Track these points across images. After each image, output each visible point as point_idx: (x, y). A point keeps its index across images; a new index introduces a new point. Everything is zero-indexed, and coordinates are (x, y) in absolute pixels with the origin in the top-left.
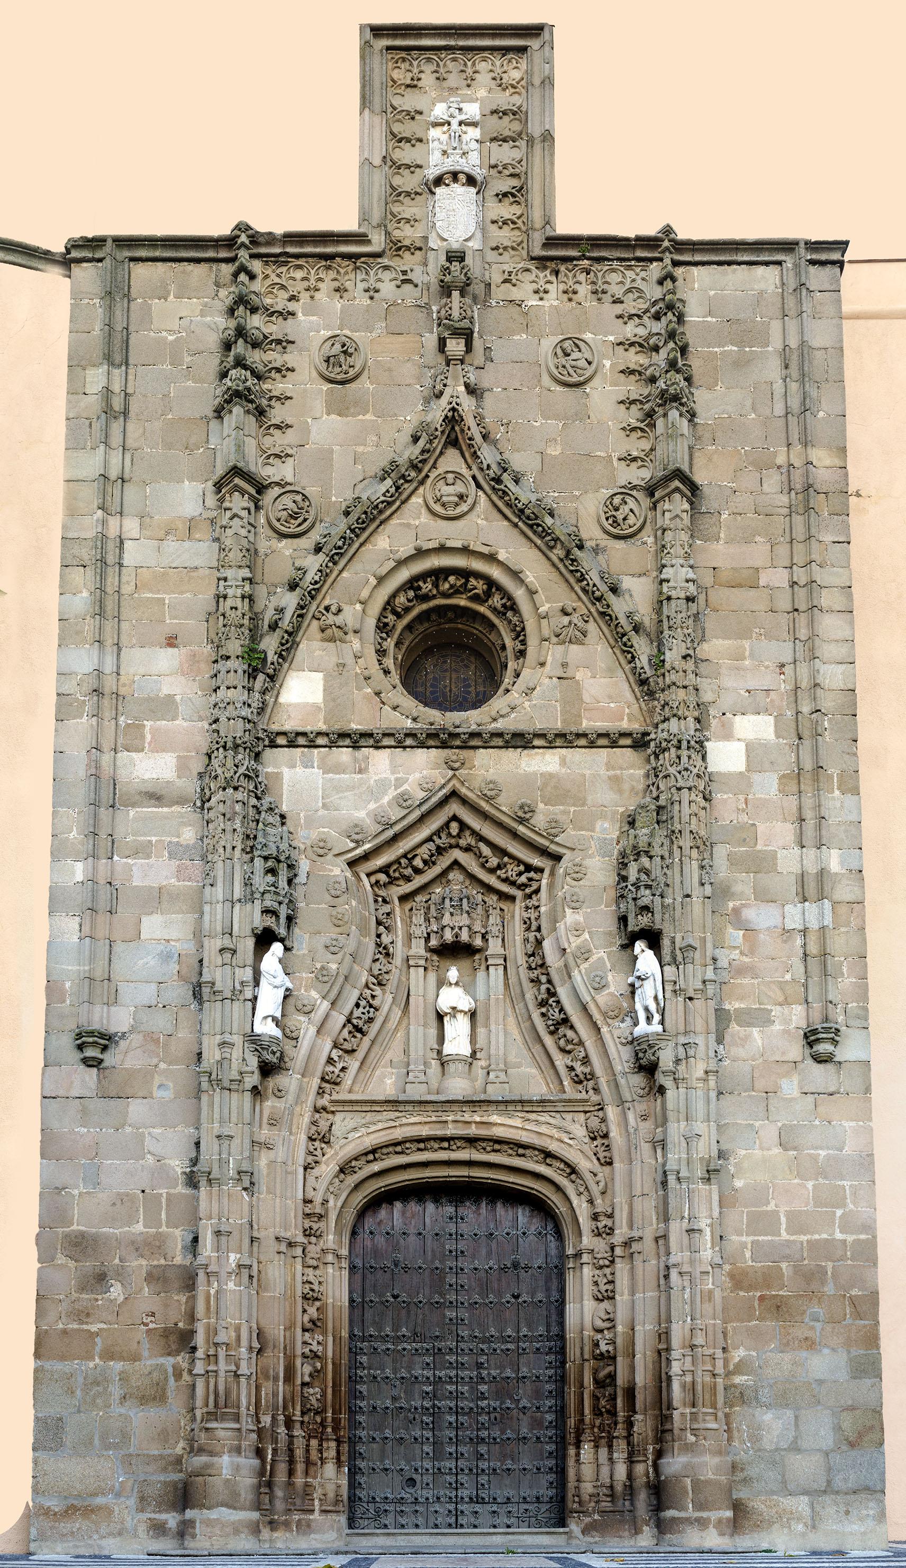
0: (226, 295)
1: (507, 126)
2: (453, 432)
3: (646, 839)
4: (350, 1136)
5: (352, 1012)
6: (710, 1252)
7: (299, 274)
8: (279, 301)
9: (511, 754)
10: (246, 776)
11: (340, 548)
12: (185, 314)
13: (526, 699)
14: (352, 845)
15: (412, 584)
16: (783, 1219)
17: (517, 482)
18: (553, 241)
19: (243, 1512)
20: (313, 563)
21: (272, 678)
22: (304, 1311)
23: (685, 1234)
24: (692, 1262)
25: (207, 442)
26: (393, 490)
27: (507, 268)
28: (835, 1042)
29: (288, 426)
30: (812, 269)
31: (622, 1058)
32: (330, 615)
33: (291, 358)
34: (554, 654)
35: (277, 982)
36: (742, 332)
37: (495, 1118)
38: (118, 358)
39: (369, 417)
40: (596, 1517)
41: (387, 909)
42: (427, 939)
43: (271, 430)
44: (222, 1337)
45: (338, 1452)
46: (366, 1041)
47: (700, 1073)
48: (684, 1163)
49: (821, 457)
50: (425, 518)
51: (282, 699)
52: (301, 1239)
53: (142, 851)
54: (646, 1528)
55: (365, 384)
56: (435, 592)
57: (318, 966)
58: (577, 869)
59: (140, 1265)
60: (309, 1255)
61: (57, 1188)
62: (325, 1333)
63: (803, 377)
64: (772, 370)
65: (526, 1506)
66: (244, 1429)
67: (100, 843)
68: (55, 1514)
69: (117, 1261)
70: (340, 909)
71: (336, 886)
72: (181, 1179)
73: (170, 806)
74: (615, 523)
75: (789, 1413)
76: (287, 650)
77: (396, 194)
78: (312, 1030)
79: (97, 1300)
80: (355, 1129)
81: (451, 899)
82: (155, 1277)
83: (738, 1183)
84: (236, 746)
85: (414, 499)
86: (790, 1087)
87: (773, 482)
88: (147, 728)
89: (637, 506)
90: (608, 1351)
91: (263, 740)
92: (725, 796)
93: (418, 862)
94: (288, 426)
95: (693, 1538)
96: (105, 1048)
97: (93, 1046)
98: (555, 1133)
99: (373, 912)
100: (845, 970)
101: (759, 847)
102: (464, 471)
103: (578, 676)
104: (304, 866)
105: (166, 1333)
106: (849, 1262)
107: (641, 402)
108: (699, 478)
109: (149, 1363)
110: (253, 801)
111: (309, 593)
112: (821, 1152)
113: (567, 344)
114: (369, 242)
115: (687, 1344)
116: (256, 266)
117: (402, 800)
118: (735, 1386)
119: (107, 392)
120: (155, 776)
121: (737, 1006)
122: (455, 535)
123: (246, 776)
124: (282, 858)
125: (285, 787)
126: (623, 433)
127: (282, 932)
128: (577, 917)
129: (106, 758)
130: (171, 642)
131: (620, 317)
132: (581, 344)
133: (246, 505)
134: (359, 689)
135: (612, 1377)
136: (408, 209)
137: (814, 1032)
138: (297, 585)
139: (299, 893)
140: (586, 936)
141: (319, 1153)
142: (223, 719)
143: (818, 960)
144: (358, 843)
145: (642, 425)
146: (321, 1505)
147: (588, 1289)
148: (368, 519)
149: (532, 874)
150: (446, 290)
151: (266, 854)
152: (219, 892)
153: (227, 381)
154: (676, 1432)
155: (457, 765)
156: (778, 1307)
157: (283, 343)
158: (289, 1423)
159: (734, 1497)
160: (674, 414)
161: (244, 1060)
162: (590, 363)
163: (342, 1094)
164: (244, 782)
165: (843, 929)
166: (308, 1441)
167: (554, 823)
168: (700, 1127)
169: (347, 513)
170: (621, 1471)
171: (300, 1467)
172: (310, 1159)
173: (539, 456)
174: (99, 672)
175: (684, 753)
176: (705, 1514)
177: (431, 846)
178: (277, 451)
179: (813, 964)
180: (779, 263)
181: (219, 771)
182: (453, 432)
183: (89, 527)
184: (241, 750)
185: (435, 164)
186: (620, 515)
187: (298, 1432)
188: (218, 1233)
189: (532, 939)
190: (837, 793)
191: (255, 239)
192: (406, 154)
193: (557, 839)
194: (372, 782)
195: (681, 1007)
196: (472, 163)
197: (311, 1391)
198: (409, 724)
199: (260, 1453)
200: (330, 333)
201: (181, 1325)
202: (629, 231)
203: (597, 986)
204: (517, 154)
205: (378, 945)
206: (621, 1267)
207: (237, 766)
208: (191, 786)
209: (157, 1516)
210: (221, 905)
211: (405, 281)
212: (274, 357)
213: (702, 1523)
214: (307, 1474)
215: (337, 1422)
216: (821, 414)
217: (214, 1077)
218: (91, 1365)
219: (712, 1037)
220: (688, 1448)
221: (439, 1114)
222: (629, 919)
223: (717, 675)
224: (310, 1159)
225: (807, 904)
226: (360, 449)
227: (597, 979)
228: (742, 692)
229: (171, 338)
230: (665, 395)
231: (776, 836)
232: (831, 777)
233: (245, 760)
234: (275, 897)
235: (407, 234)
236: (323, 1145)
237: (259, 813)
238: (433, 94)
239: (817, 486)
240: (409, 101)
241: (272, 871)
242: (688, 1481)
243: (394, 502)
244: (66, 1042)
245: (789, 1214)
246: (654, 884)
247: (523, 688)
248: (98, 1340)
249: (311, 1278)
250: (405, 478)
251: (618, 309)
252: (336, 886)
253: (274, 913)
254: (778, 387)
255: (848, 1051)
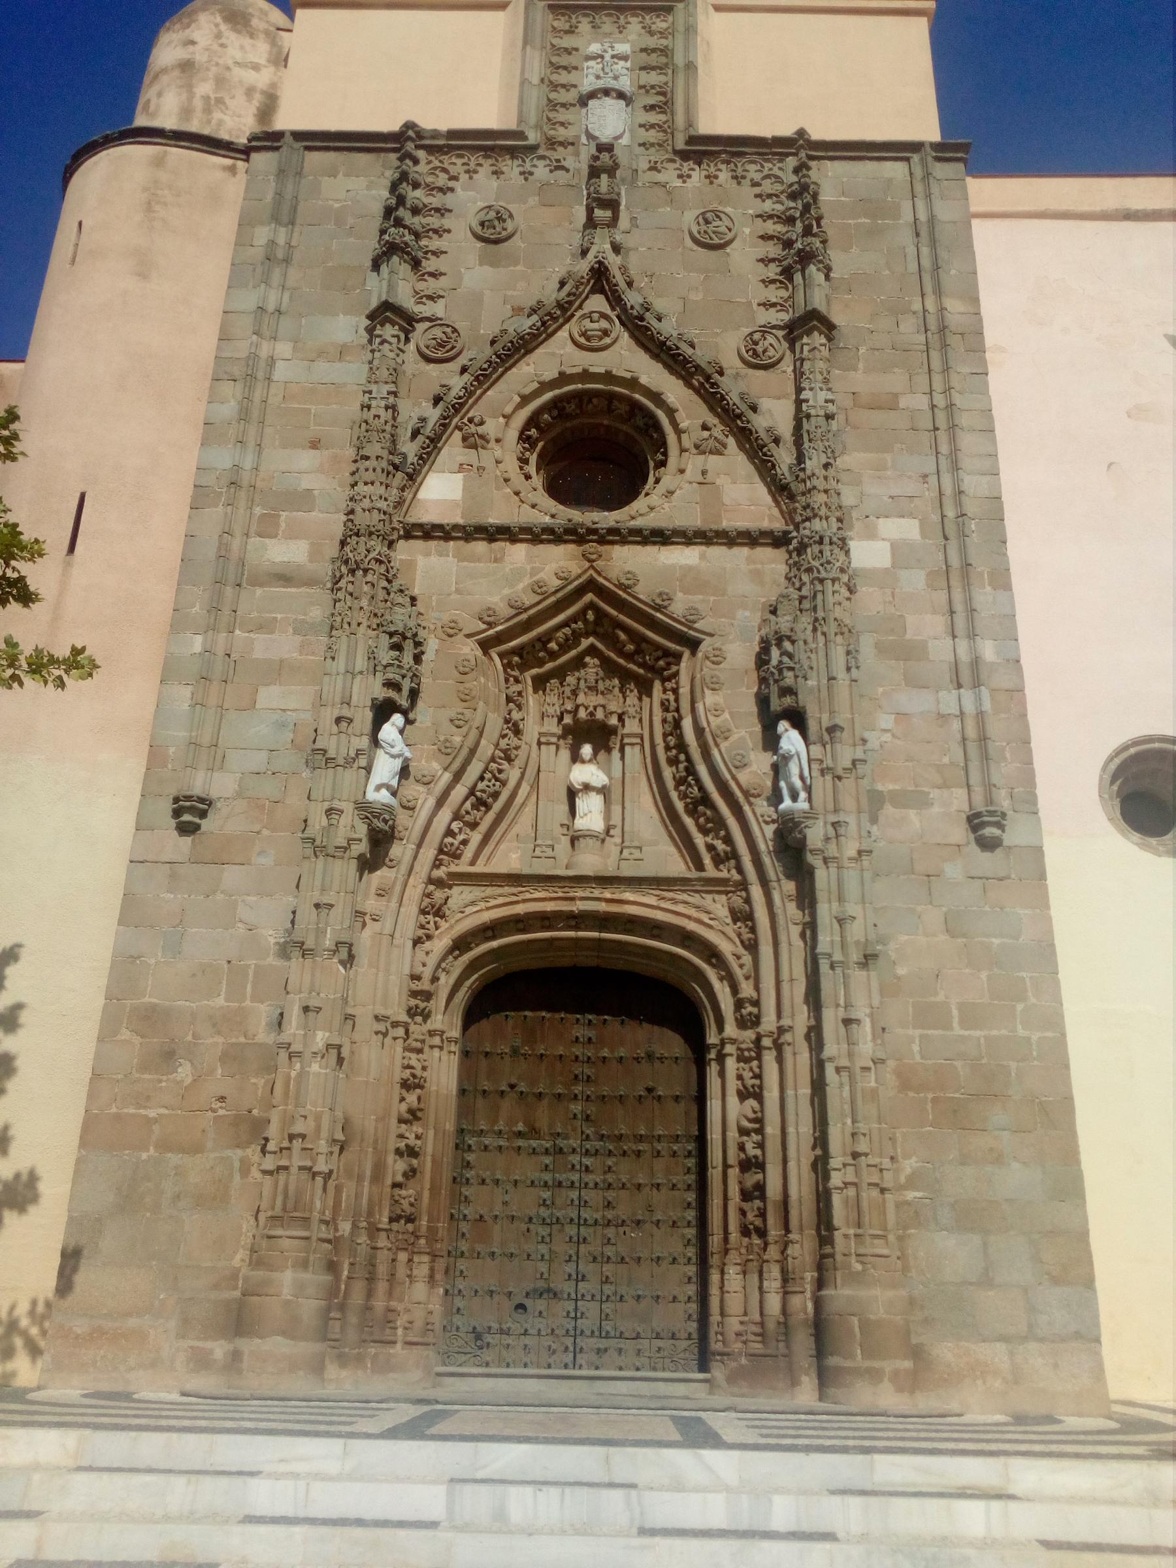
0: (390, 175)
1: (654, 59)
2: (600, 277)
3: (788, 625)
4: (468, 910)
5: (475, 785)
6: (870, 1045)
7: (459, 161)
8: (442, 180)
9: (651, 550)
10: (377, 560)
11: (485, 370)
12: (362, 187)
13: (665, 500)
14: (484, 626)
15: (555, 404)
16: (955, 1013)
17: (660, 320)
18: (693, 140)
19: (303, 1344)
20: (458, 383)
21: (411, 477)
22: (402, 1099)
23: (841, 1025)
24: (850, 1055)
25: (364, 284)
26: (539, 324)
27: (653, 158)
28: (1001, 826)
29: (442, 274)
30: (938, 165)
31: (764, 836)
32: (472, 426)
33: (447, 222)
34: (694, 463)
35: (395, 751)
36: (876, 209)
37: (628, 896)
38: (285, 219)
39: (519, 268)
40: (744, 1361)
41: (518, 687)
42: (561, 719)
43: (426, 277)
44: (299, 1128)
45: (432, 1269)
46: (491, 816)
47: (852, 853)
48: (838, 947)
49: (955, 307)
50: (570, 348)
51: (421, 495)
52: (404, 1018)
53: (262, 627)
54: (805, 1379)
55: (516, 241)
56: (578, 411)
57: (442, 738)
58: (717, 653)
59: (214, 1043)
60: (413, 1037)
61: (132, 957)
62: (425, 1127)
63: (933, 243)
64: (906, 238)
65: (660, 1343)
66: (314, 1238)
67: (219, 615)
68: (77, 1337)
69: (190, 1038)
70: (467, 685)
71: (465, 663)
72: (273, 949)
73: (298, 587)
74: (755, 354)
75: (976, 1240)
76: (427, 456)
77: (553, 105)
78: (431, 802)
79: (160, 1081)
80: (473, 903)
81: (586, 680)
82: (232, 1057)
83: (901, 971)
84: (371, 534)
85: (559, 333)
86: (953, 871)
87: (909, 325)
88: (282, 518)
89: (774, 344)
90: (756, 1157)
91: (398, 530)
92: (871, 590)
93: (553, 645)
94: (442, 274)
95: (864, 1395)
96: (203, 814)
97: (190, 813)
98: (692, 912)
99: (503, 689)
100: (1008, 755)
101: (908, 637)
102: (608, 311)
103: (718, 482)
104: (432, 646)
105: (236, 1121)
106: (1036, 1063)
107: (780, 261)
108: (836, 319)
109: (213, 1155)
110: (385, 584)
111: (453, 406)
112: (994, 940)
113: (709, 215)
114: (526, 138)
115: (849, 1151)
116: (421, 154)
117: (537, 587)
118: (908, 1203)
119: (272, 243)
120: (286, 559)
121: (891, 787)
122: (598, 363)
123: (377, 560)
124: (409, 635)
125: (418, 572)
126: (761, 284)
127: (404, 703)
128: (717, 697)
129: (236, 544)
130: (315, 445)
131: (756, 196)
132: (722, 216)
133: (396, 333)
134: (497, 488)
135: (760, 1188)
136: (562, 115)
137: (978, 815)
138: (441, 399)
139: (424, 668)
140: (726, 715)
141: (432, 926)
142: (358, 510)
143: (979, 745)
144: (490, 625)
145: (781, 278)
146: (405, 1335)
147: (732, 1085)
148: (514, 349)
149: (671, 659)
150: (594, 173)
151: (392, 629)
152: (341, 664)
153: (386, 237)
154: (839, 1257)
155: (594, 557)
156: (955, 1111)
157: (441, 211)
158: (373, 1231)
159: (914, 1341)
160: (812, 268)
161: (353, 826)
162: (730, 230)
163: (462, 867)
164: (373, 565)
165: (1003, 716)
166: (395, 1254)
167: (693, 610)
168: (853, 909)
169: (493, 342)
170: (774, 1303)
171: (382, 1287)
172: (421, 932)
173: (681, 302)
174: (237, 467)
175: (827, 548)
176: (876, 1364)
177: (567, 630)
178: (429, 293)
179: (973, 749)
180: (907, 159)
181: (351, 555)
182: (600, 277)
183: (242, 349)
184: (374, 537)
185: (588, 83)
186: (759, 349)
187: (382, 1241)
188: (306, 1009)
189: (670, 719)
190: (988, 589)
191: (420, 134)
192: (563, 77)
193: (696, 625)
194: (507, 570)
195: (829, 785)
196: (625, 84)
197: (404, 1193)
198: (547, 519)
199: (332, 1267)
200: (486, 204)
201: (255, 1112)
202: (767, 132)
203: (738, 764)
204: (663, 78)
205: (507, 721)
206: (769, 1058)
207: (369, 551)
208: (325, 570)
209: (201, 1344)
210: (341, 676)
211: (558, 168)
212: (434, 221)
213: (875, 1376)
214: (390, 1294)
215: (432, 1230)
216: (953, 272)
217: (318, 843)
218: (144, 1156)
219: (865, 817)
220: (856, 1279)
221: (566, 889)
222: (772, 699)
223: (858, 483)
224: (421, 932)
225: (962, 690)
226: (509, 293)
227: (739, 758)
228: (885, 498)
229: (337, 205)
230: (798, 250)
231: (927, 627)
232: (981, 574)
233: (378, 547)
234: (398, 670)
235: (561, 133)
236: (437, 919)
237: (389, 594)
238: (589, 37)
239: (953, 328)
240: (567, 42)
241: (397, 647)
242: (855, 1321)
243: (540, 335)
244: (165, 807)
245: (961, 1007)
246: (797, 666)
247: (663, 491)
248: (156, 1128)
249: (413, 1063)
250: (551, 319)
251: (757, 190)
252: (465, 663)
253: (397, 687)
254: (911, 250)
255: (1014, 835)
